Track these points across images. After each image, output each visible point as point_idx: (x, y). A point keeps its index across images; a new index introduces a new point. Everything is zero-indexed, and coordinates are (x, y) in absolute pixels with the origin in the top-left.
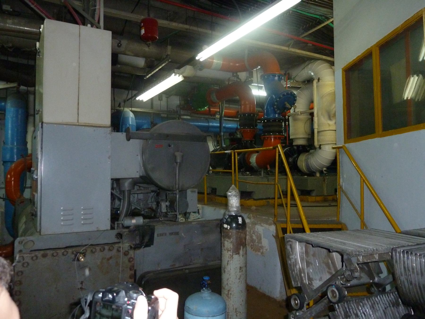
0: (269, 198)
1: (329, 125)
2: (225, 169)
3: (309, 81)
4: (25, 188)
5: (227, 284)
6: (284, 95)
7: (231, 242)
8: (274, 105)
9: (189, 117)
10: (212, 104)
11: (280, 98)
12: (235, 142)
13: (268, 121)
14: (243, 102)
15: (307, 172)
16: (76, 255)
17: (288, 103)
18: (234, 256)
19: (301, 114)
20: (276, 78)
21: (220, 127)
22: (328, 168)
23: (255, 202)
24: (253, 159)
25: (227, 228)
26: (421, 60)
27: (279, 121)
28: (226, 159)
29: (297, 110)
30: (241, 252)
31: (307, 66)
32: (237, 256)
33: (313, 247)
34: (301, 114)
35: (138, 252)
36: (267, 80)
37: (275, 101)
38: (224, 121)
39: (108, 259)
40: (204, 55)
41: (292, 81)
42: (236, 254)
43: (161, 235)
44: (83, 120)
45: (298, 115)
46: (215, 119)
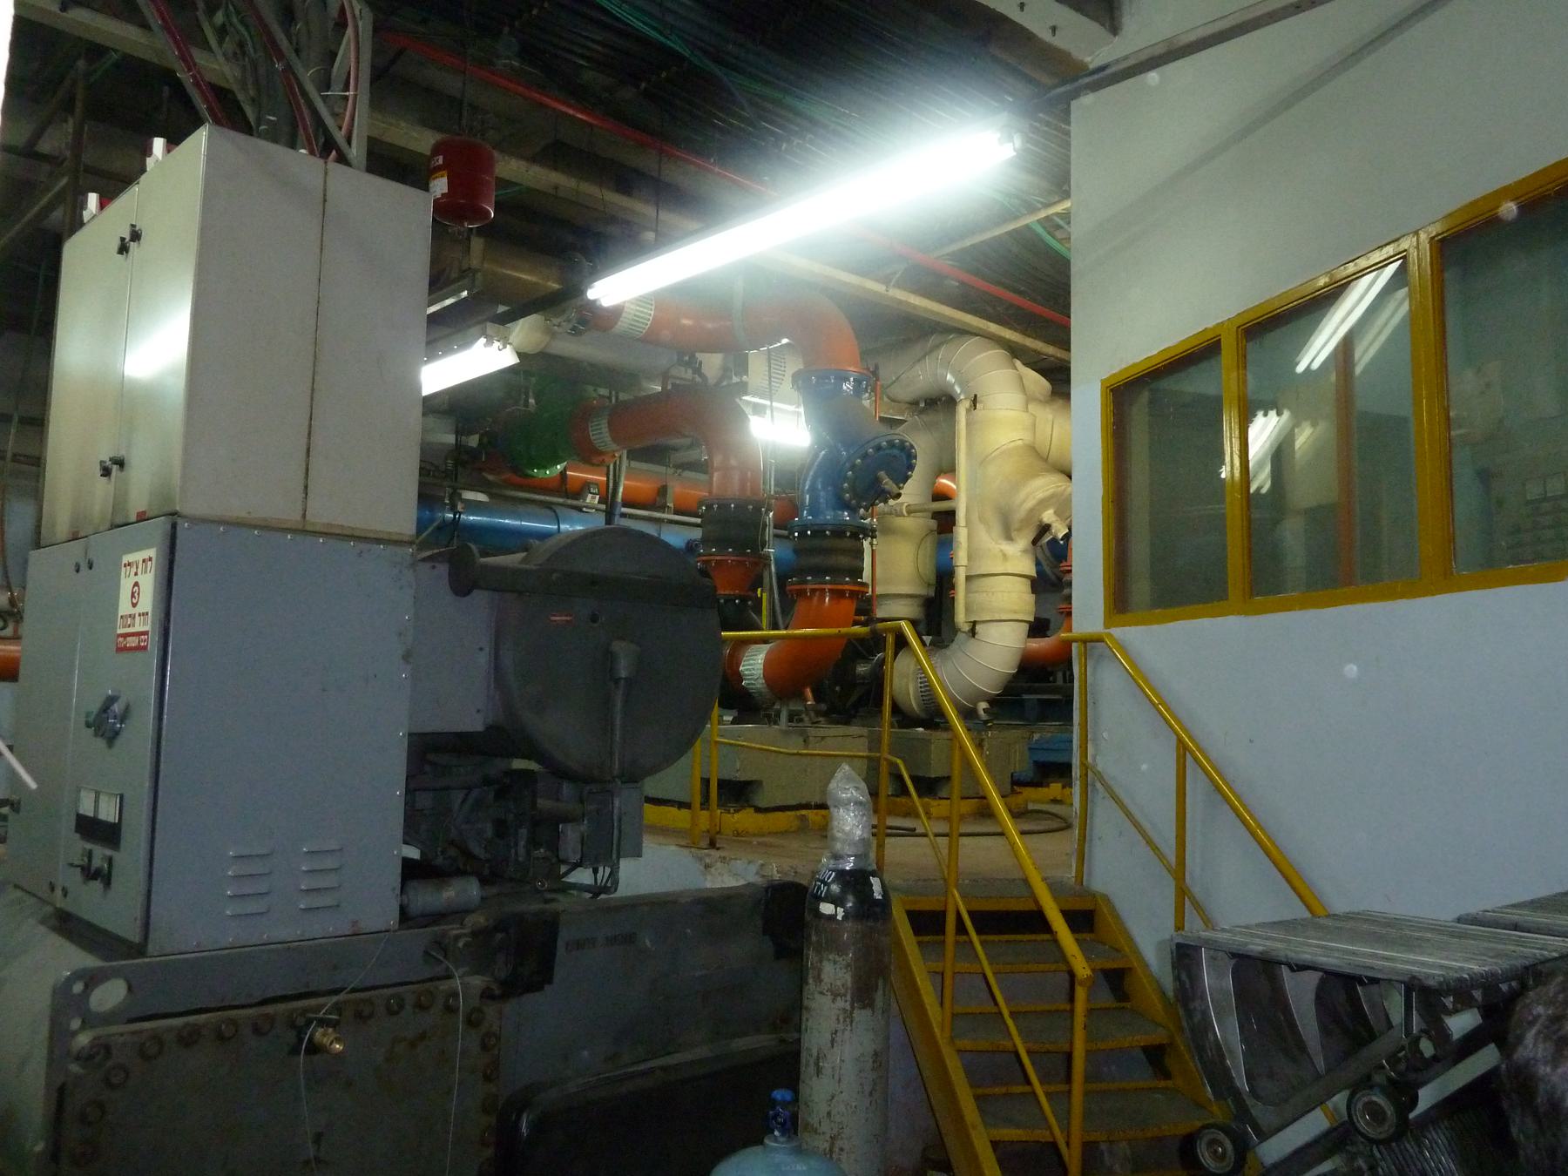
0: (807, 806)
1: (1005, 556)
5: (829, 1114)
6: (878, 448)
7: (848, 965)
8: (846, 479)
9: (482, 497)
10: (589, 455)
11: (865, 456)
13: (819, 533)
15: (923, 715)
16: (300, 1032)
18: (856, 1012)
19: (909, 512)
20: (847, 387)
22: (994, 702)
23: (760, 817)
24: (754, 665)
25: (832, 917)
26: (1300, 368)
27: (855, 536)
30: (879, 998)
31: (931, 351)
32: (868, 1012)
33: (1292, 970)
34: (909, 512)
35: (510, 1007)
36: (817, 386)
39: (412, 1045)
40: (618, 288)
42: (864, 1007)
43: (579, 945)
44: (323, 512)
46: (579, 509)
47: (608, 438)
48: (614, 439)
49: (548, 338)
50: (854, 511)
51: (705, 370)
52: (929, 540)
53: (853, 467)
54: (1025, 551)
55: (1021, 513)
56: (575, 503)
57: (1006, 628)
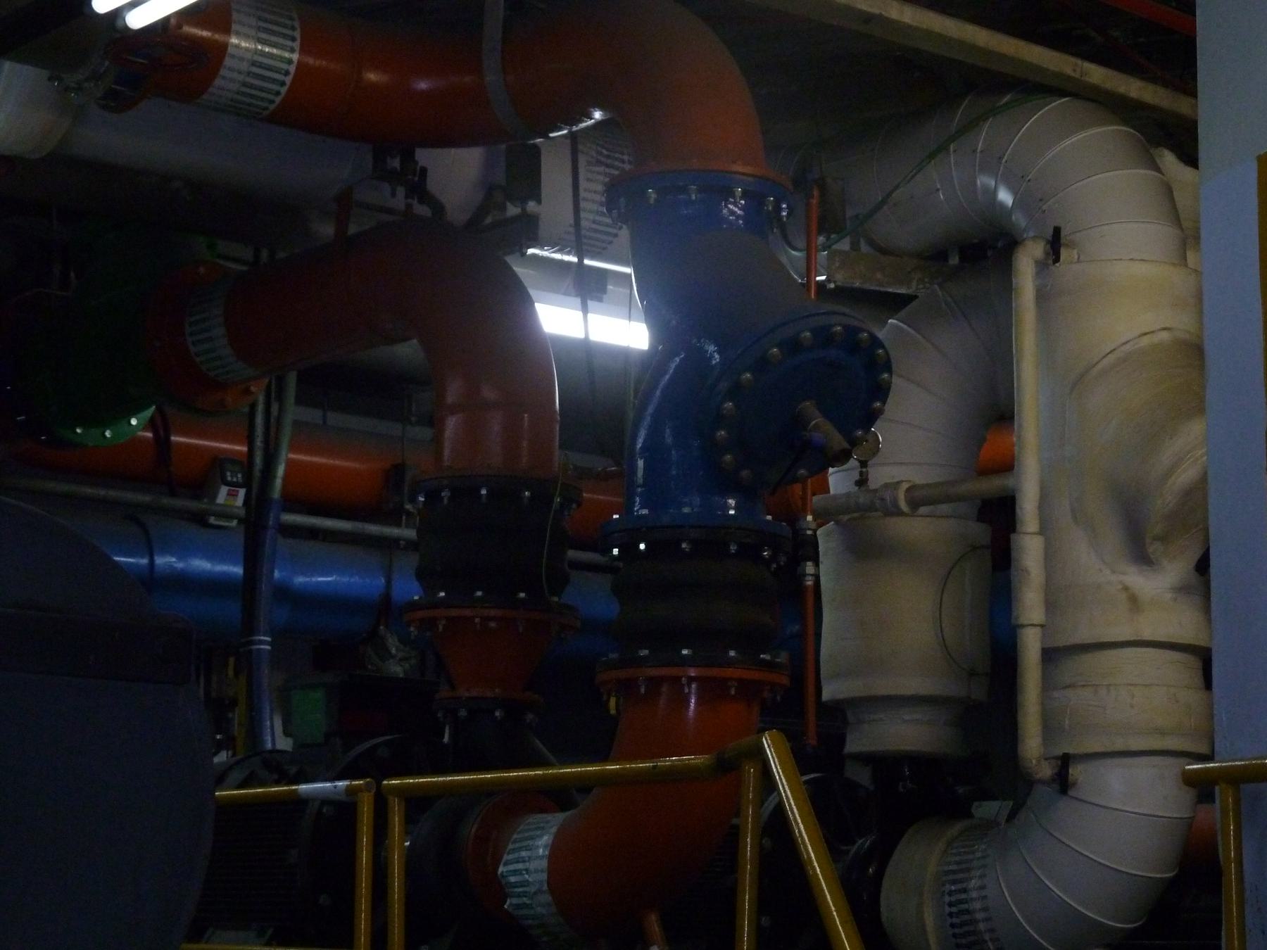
1: (1134, 602)
6: (793, 346)
10: (189, 392)
11: (762, 365)
19: (915, 504)
20: (734, 209)
34: (915, 504)
46: (200, 519)
51: (433, 185)
54: (1182, 589)
55: (1166, 499)
56: (193, 505)
57: (1144, 770)
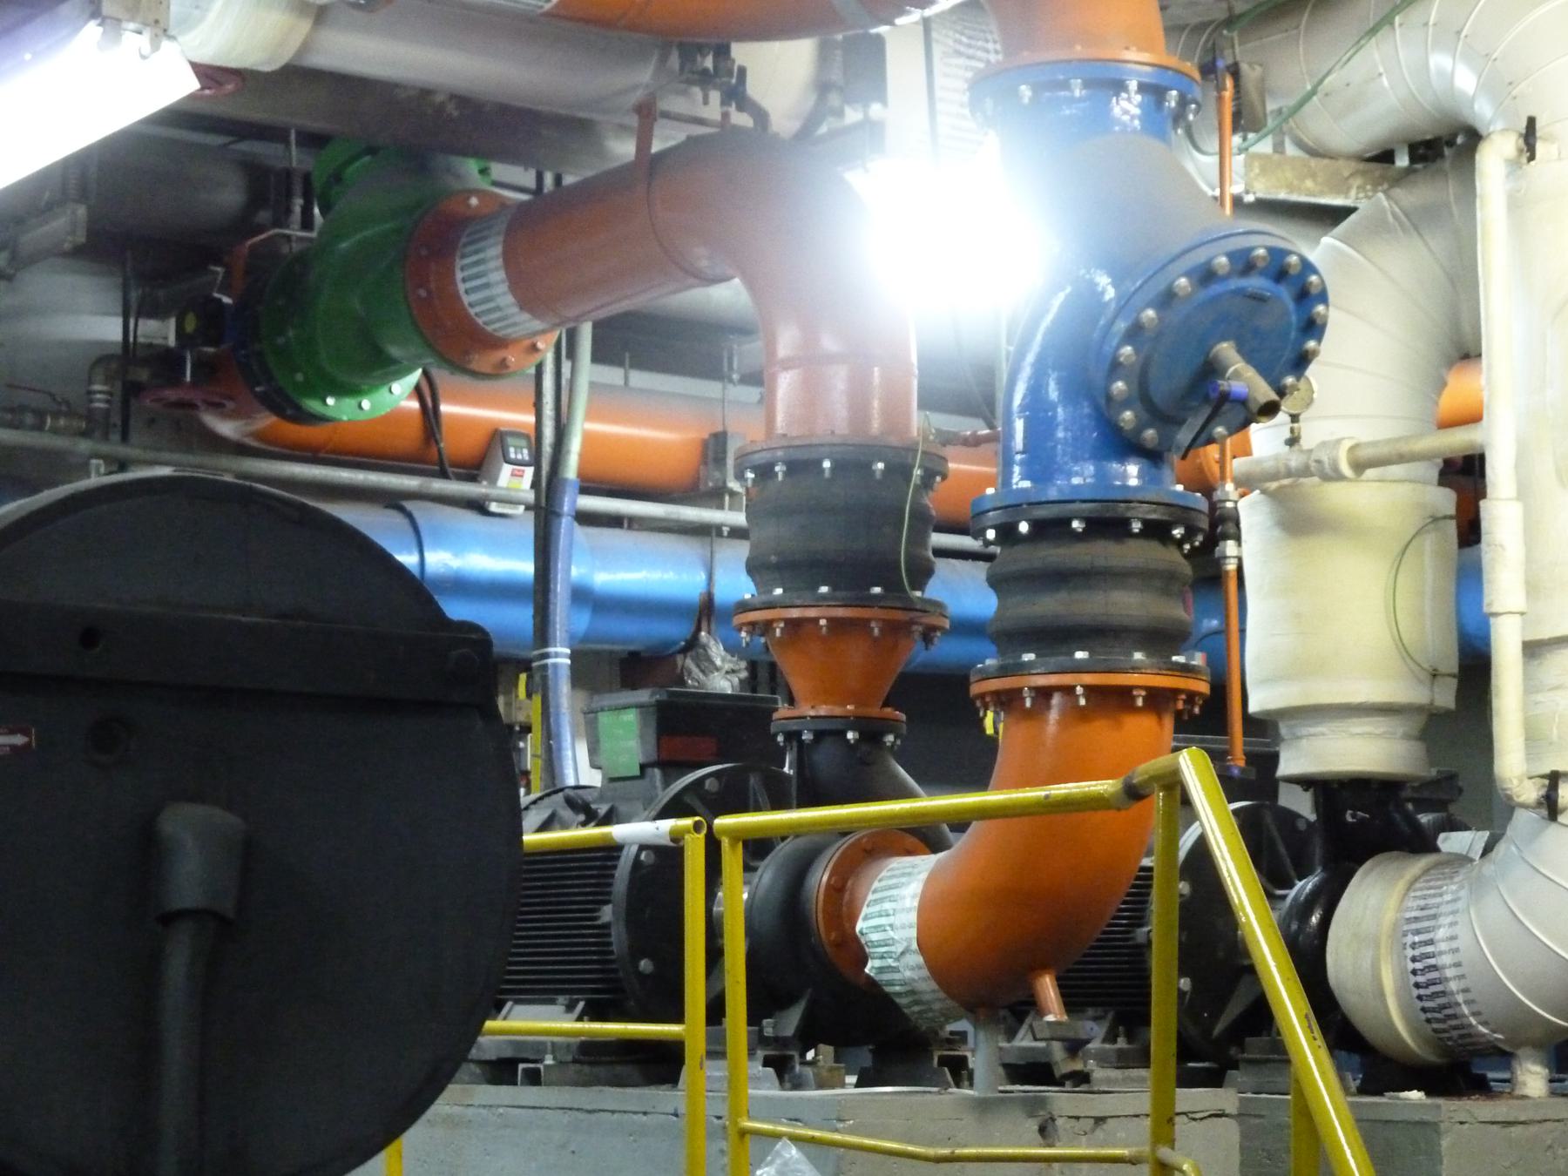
2: (596, 1012)
3: (1437, 150)
4: (465, 1060)
6: (1206, 275)
8: (1115, 368)
10: (461, 345)
11: (1167, 299)
12: (711, 743)
13: (1051, 528)
14: (787, 341)
17: (1249, 356)
21: (541, 588)
24: (894, 914)
28: (607, 913)
29: (1314, 432)
34: (1359, 466)
37: (1122, 325)
38: (582, 534)
41: (1265, 146)
45: (1336, 476)
46: (478, 506)
47: (507, 300)
48: (525, 304)
49: (304, 26)
50: (1153, 457)
52: (1428, 543)
53: (1135, 333)
